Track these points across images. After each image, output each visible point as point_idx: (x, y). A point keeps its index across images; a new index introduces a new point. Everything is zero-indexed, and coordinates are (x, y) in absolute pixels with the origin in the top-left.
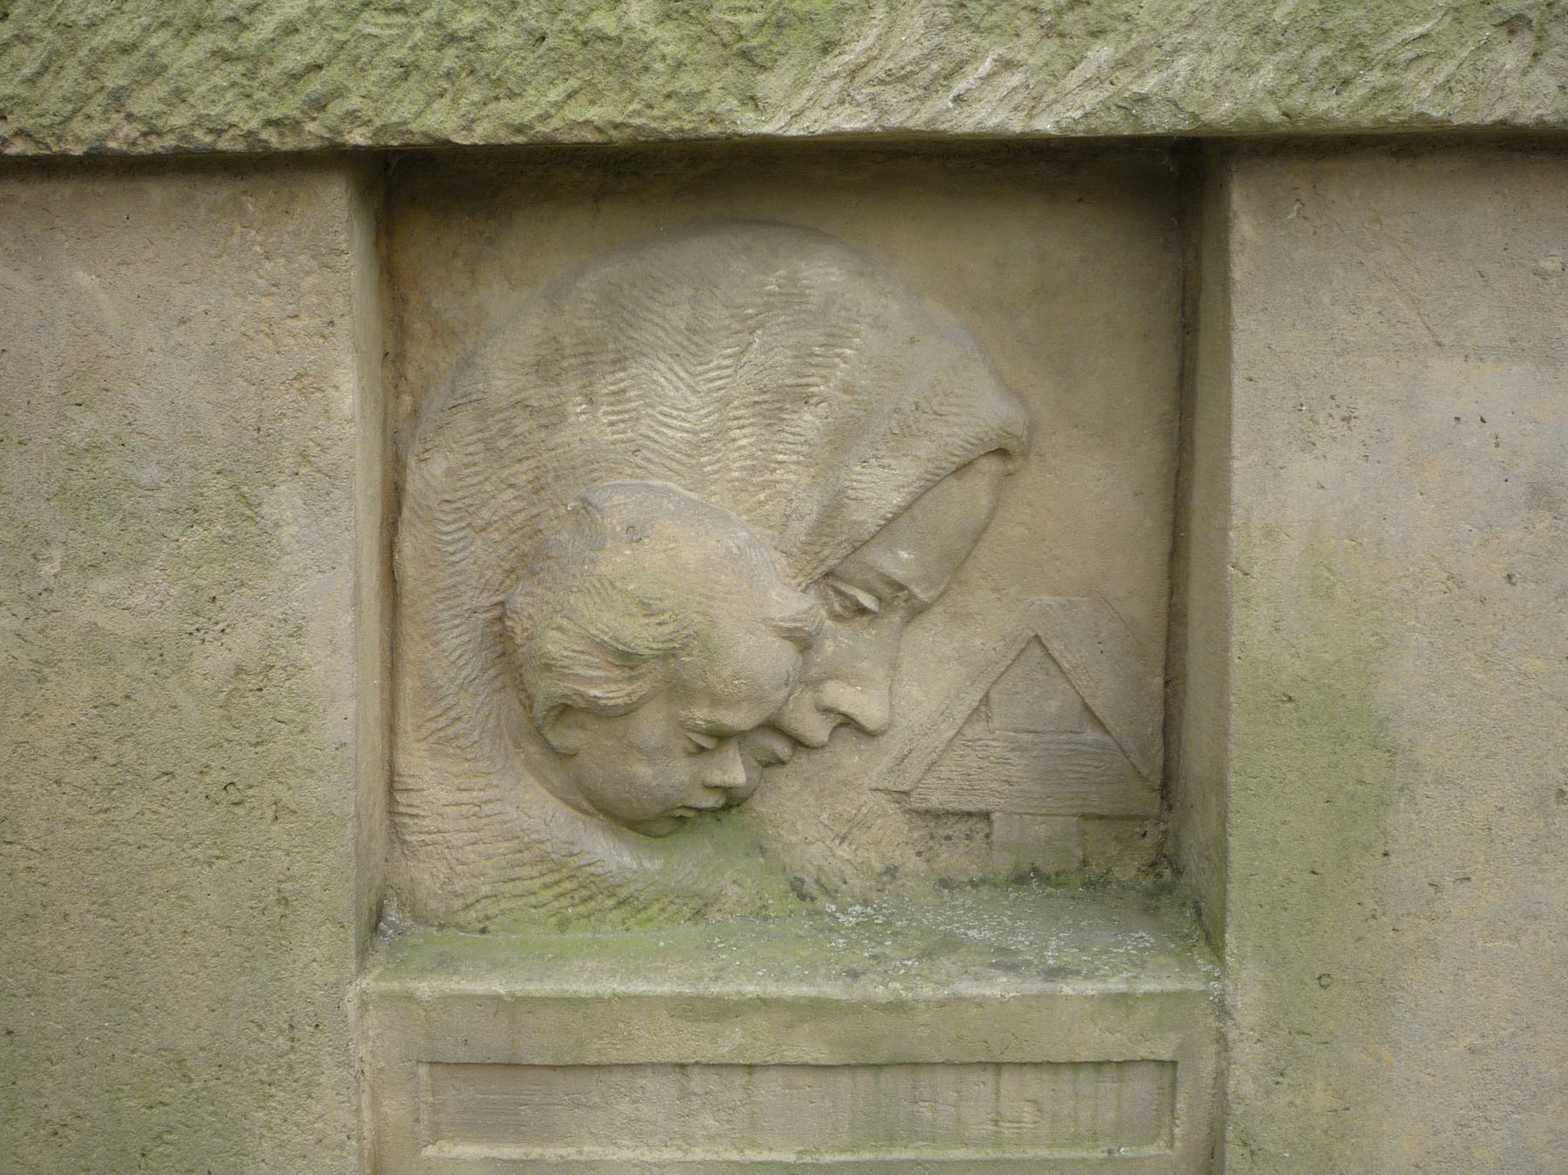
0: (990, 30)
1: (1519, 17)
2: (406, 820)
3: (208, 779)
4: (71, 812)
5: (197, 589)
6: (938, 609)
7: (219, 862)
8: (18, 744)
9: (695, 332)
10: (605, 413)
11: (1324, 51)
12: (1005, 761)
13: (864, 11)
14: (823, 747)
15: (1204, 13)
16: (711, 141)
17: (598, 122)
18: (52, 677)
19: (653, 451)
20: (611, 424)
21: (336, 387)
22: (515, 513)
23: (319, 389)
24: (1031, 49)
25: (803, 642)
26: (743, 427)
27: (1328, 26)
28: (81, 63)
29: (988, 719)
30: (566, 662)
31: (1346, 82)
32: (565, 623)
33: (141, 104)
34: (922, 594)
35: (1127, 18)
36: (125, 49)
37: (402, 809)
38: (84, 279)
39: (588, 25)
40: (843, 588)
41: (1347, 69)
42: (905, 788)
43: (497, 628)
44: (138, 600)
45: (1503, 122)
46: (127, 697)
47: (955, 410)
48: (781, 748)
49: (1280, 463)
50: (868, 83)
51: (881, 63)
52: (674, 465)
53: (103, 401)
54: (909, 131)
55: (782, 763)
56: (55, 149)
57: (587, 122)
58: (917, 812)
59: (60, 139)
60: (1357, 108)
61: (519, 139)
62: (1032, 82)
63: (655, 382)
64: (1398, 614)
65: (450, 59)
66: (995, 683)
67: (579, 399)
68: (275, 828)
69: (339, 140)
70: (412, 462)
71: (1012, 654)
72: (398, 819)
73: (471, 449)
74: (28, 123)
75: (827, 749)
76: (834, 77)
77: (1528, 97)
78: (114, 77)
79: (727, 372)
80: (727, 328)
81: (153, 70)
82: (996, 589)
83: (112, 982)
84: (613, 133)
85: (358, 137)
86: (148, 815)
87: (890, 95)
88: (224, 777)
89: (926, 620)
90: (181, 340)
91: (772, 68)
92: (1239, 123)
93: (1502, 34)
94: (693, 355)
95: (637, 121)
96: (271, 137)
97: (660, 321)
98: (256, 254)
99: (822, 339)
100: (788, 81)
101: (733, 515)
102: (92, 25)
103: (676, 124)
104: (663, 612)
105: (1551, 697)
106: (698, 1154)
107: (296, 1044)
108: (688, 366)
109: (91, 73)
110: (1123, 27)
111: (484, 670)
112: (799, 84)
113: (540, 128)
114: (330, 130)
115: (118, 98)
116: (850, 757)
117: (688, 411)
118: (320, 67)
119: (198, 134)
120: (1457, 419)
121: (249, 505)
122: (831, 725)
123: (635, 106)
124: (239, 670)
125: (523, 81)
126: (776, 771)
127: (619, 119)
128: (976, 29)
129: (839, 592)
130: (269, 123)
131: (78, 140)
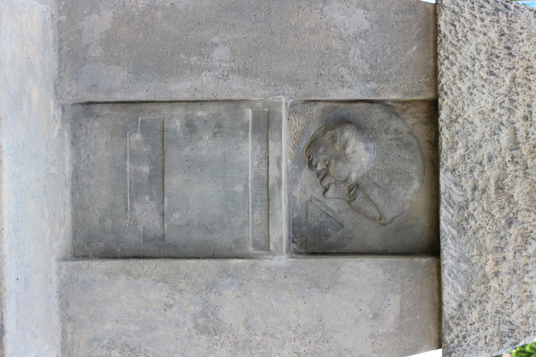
0: (458, 213)
1: (462, 306)
2: (309, 104)
3: (322, 70)
4: (316, 45)
5: (357, 69)
6: (349, 207)
7: (307, 72)
8: (329, 35)
9: (404, 160)
10: (388, 143)
11: (455, 271)
12: (318, 221)
13: (462, 191)
14: (321, 184)
15: (462, 251)
16: (439, 164)
17: (442, 144)
18: (341, 42)
19: (381, 152)
20: (386, 144)
21: (394, 95)
22: (369, 125)
23: (394, 92)
24: (455, 220)
25: (346, 180)
26: (386, 169)
27: (460, 272)
28: (454, 51)
29: (326, 218)
30: (343, 136)
31: (450, 275)
32: (350, 136)
33: (446, 62)
34: (353, 204)
35: (461, 237)
36: (456, 59)
37: (311, 103)
38: (415, 48)
39: (459, 142)
40: (355, 188)
41: (452, 276)
42: (312, 201)
43: (346, 121)
44: (356, 58)
45: (443, 304)
46: (337, 56)
47: (389, 209)
48: (321, 177)
49: (381, 267)
50: (449, 191)
51: (453, 194)
52: (379, 156)
53: (392, 52)
54: (441, 199)
55: (318, 176)
56: (438, 46)
57: (442, 142)
58: (307, 203)
59: (440, 47)
60: (445, 277)
61: (439, 129)
62: (449, 220)
63: (394, 152)
64: (354, 289)
65: (454, 117)
66: (334, 218)
67: (391, 137)
68: (313, 83)
69: (439, 97)
70: (378, 105)
71: (340, 222)
72: (309, 102)
73: (381, 117)
74: (443, 41)
75: (320, 185)
76: (450, 185)
77: (448, 308)
78: (451, 57)
79: (396, 166)
80: (405, 166)
81: (452, 64)
82: (353, 218)
83: (284, 52)
84: (440, 146)
85: (440, 101)
86: (316, 59)
87: (447, 195)
88: (323, 74)
89: (347, 204)
90: (403, 66)
91: (452, 174)
92: (443, 257)
93: (459, 304)
94: (400, 159)
95: (442, 151)
96: (440, 85)
97: (406, 153)
98: (419, 80)
99: (403, 184)
100: (449, 177)
101: (369, 167)
102: (461, 53)
103: (442, 157)
104: (353, 154)
105: (338, 318)
106: (250, 161)
107: (272, 86)
108: (367, 111)
109: (452, 53)
110: (459, 236)
111: (338, 119)
112: (449, 179)
113: (441, 133)
114: (441, 96)
115: (447, 58)
116: (319, 191)
117: (389, 159)
118: (452, 94)
119: (441, 72)
120: (389, 300)
121: (373, 79)
122: (326, 186)
123: (445, 150)
124: (343, 77)
125: (450, 130)
126: (316, 176)
127: (443, 147)
128: (459, 210)
129: (353, 187)
130: (443, 85)
131: (440, 50)
